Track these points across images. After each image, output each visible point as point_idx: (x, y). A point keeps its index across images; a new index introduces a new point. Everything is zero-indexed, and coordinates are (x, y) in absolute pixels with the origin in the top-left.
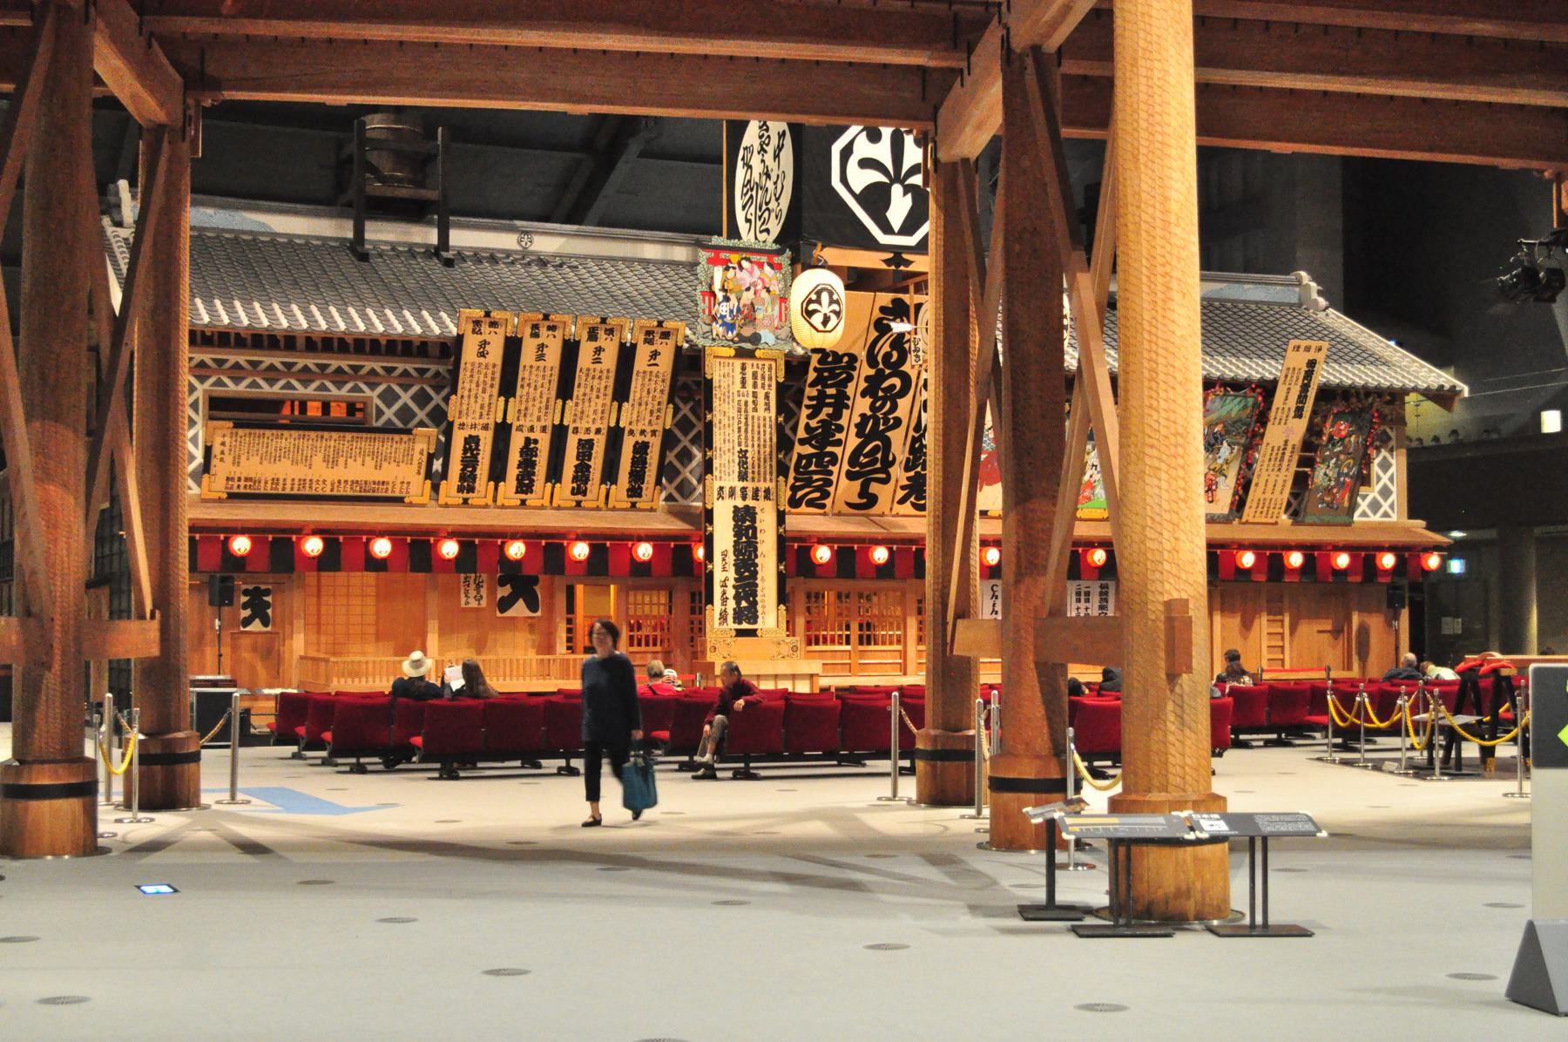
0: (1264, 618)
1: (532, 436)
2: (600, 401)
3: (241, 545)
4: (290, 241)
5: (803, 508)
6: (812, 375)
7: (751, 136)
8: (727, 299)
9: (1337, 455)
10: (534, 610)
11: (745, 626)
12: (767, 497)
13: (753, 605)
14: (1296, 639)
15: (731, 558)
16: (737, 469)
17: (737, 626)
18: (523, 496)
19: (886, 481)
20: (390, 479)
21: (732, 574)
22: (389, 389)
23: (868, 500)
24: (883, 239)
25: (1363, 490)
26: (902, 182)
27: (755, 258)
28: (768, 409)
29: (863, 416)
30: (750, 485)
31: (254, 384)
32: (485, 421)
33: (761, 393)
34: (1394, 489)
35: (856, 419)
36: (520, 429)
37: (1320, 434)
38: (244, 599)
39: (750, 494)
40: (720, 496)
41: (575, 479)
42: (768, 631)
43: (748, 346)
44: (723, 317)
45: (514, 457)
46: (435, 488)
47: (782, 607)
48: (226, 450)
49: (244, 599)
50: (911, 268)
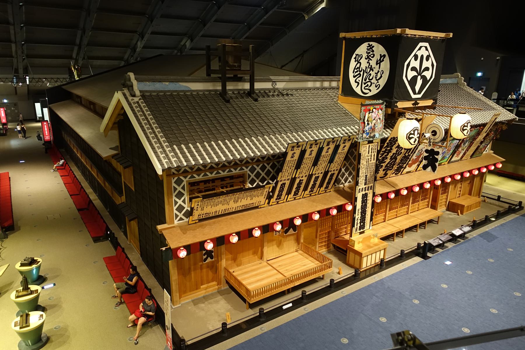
7: (362, 49)
8: (368, 124)
11: (362, 230)
12: (371, 189)
13: (364, 223)
15: (360, 210)
21: (360, 216)
22: (179, 178)
23: (386, 174)
27: (376, 107)
30: (367, 186)
43: (371, 139)
45: (295, 186)
48: (199, 207)
50: (419, 105)
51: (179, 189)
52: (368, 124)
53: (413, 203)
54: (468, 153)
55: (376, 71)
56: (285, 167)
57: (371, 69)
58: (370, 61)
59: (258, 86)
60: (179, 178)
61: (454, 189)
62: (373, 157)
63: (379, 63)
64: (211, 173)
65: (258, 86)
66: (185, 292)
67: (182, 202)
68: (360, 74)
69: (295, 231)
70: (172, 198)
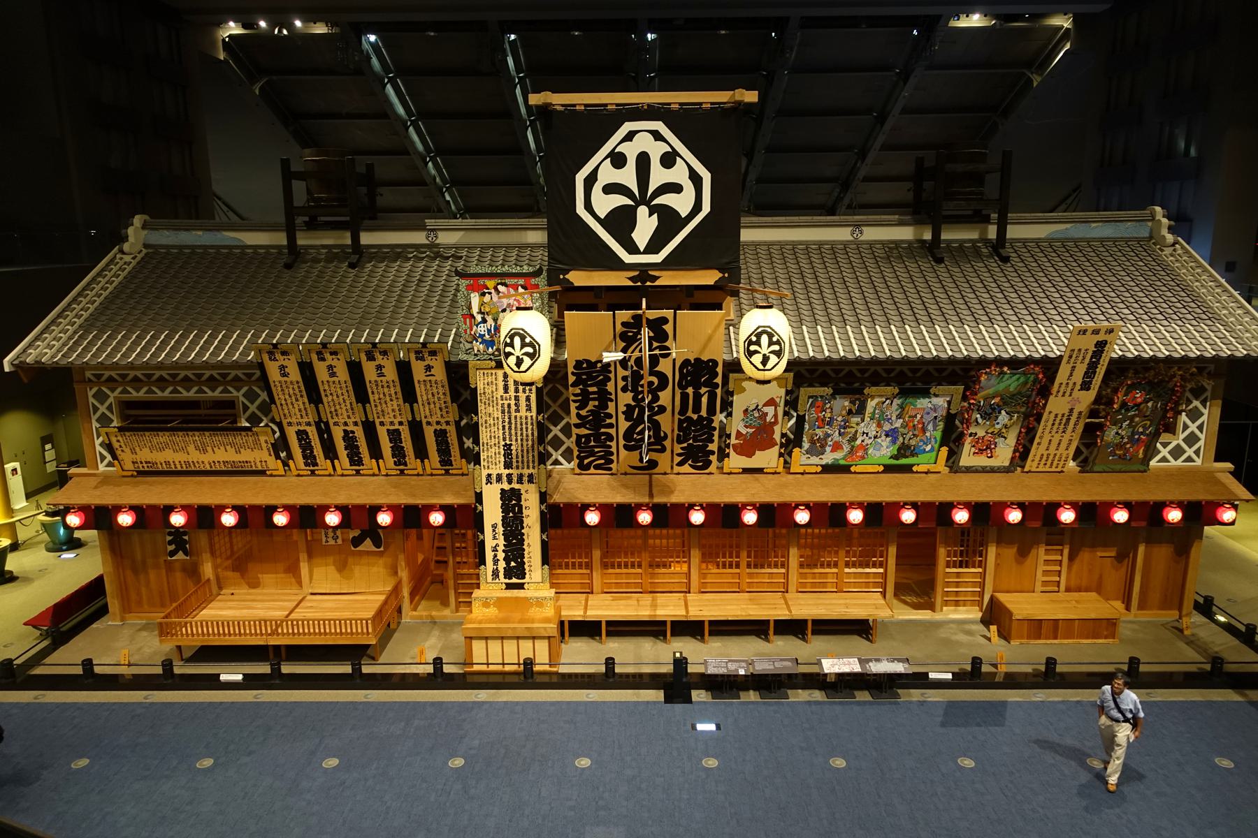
0: (1042, 550)
1: (348, 428)
2: (395, 403)
4: (255, 253)
5: (592, 470)
6: (572, 379)
8: (484, 321)
9: (1132, 419)
11: (514, 580)
12: (531, 481)
14: (1075, 567)
15: (500, 529)
16: (502, 459)
19: (663, 450)
21: (501, 541)
22: (250, 389)
24: (628, 258)
25: (1165, 437)
26: (647, 204)
27: (507, 281)
28: (529, 409)
30: (514, 472)
33: (522, 397)
34: (1202, 436)
35: (622, 408)
37: (1110, 403)
39: (515, 479)
40: (489, 481)
44: (482, 336)
47: (546, 567)
50: (657, 283)
51: (103, 409)
52: (484, 321)
59: (367, 239)
60: (100, 391)
62: (523, 403)
64: (163, 390)
65: (367, 239)
69: (377, 545)
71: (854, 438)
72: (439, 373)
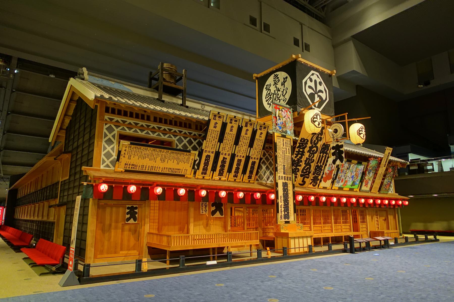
1: (225, 157)
2: (245, 147)
3: (133, 189)
6: (298, 145)
7: (270, 81)
8: (280, 119)
10: (222, 215)
11: (287, 220)
12: (290, 180)
15: (282, 198)
17: (285, 220)
18: (220, 177)
20: (181, 168)
21: (283, 204)
28: (289, 153)
29: (307, 158)
31: (136, 131)
32: (212, 150)
35: (305, 159)
36: (222, 154)
38: (128, 211)
40: (279, 179)
41: (235, 172)
42: (292, 221)
45: (219, 164)
46: (195, 173)
49: (128, 211)
51: (110, 136)
52: (280, 119)
53: (335, 223)
54: (375, 185)
55: (281, 90)
56: (209, 137)
57: (279, 90)
58: (277, 86)
61: (372, 221)
62: (288, 151)
63: (283, 84)
66: (102, 252)
67: (111, 149)
68: (271, 97)
70: (102, 142)
71: (346, 178)
72: (264, 136)
